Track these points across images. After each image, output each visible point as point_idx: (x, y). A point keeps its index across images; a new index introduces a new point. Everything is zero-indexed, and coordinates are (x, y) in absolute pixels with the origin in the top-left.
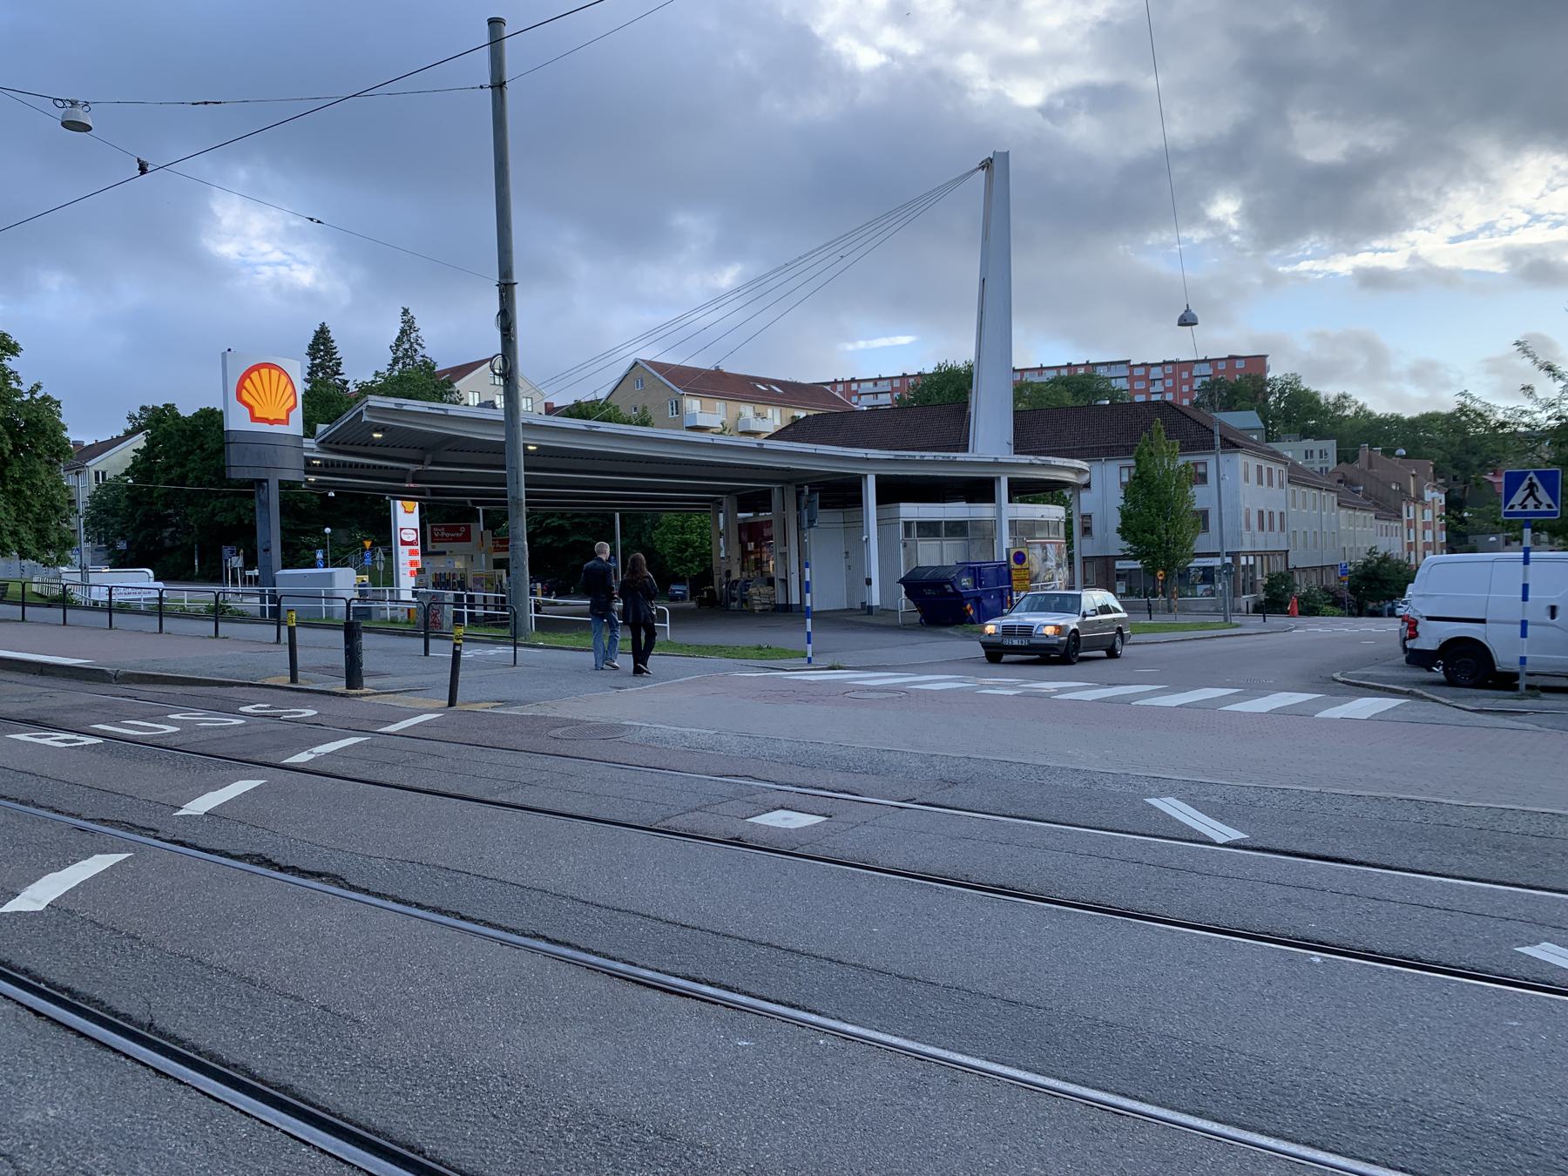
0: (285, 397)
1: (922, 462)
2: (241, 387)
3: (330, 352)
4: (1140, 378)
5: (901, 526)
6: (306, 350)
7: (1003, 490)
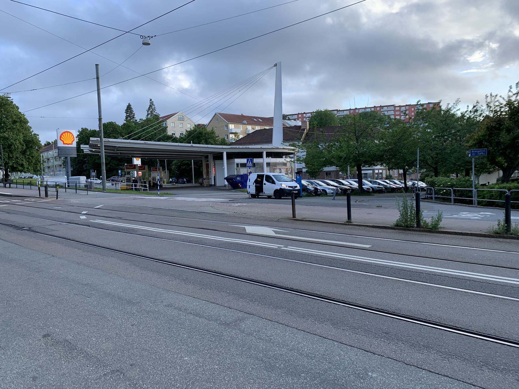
0: (72, 138)
1: (239, 148)
2: (61, 137)
3: (131, 112)
4: (398, 111)
5: (235, 165)
6: (125, 111)
7: (265, 155)
